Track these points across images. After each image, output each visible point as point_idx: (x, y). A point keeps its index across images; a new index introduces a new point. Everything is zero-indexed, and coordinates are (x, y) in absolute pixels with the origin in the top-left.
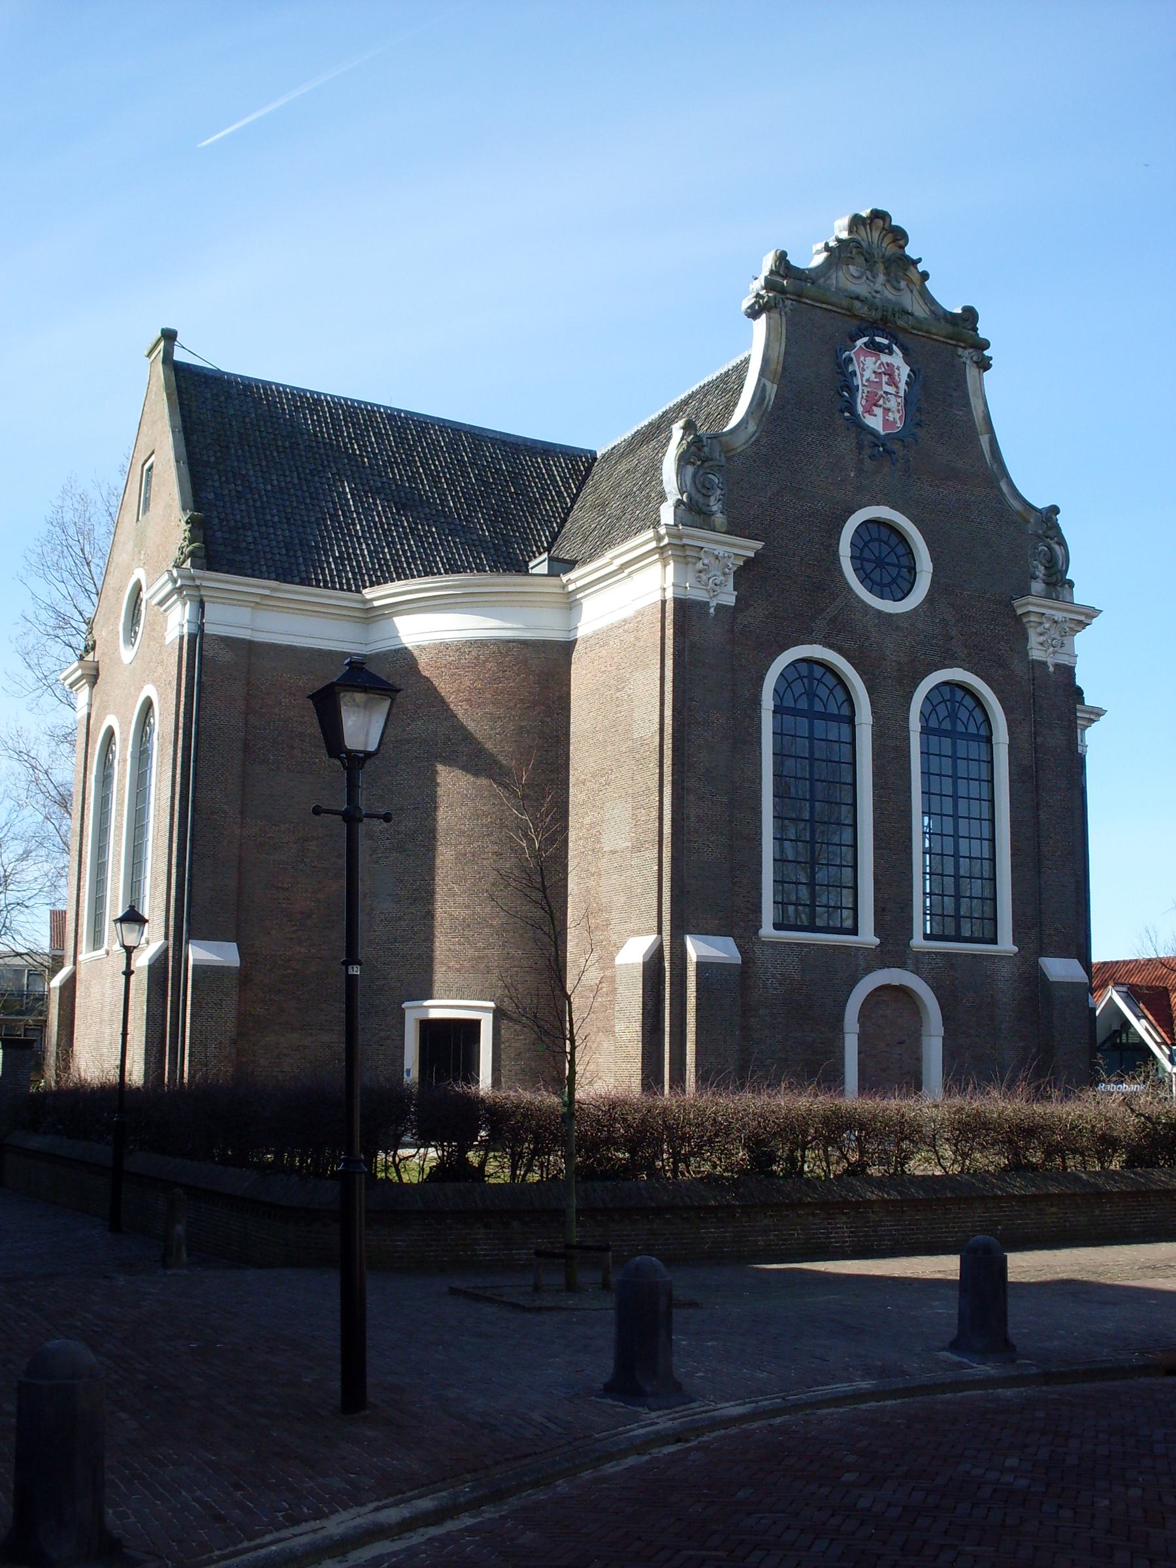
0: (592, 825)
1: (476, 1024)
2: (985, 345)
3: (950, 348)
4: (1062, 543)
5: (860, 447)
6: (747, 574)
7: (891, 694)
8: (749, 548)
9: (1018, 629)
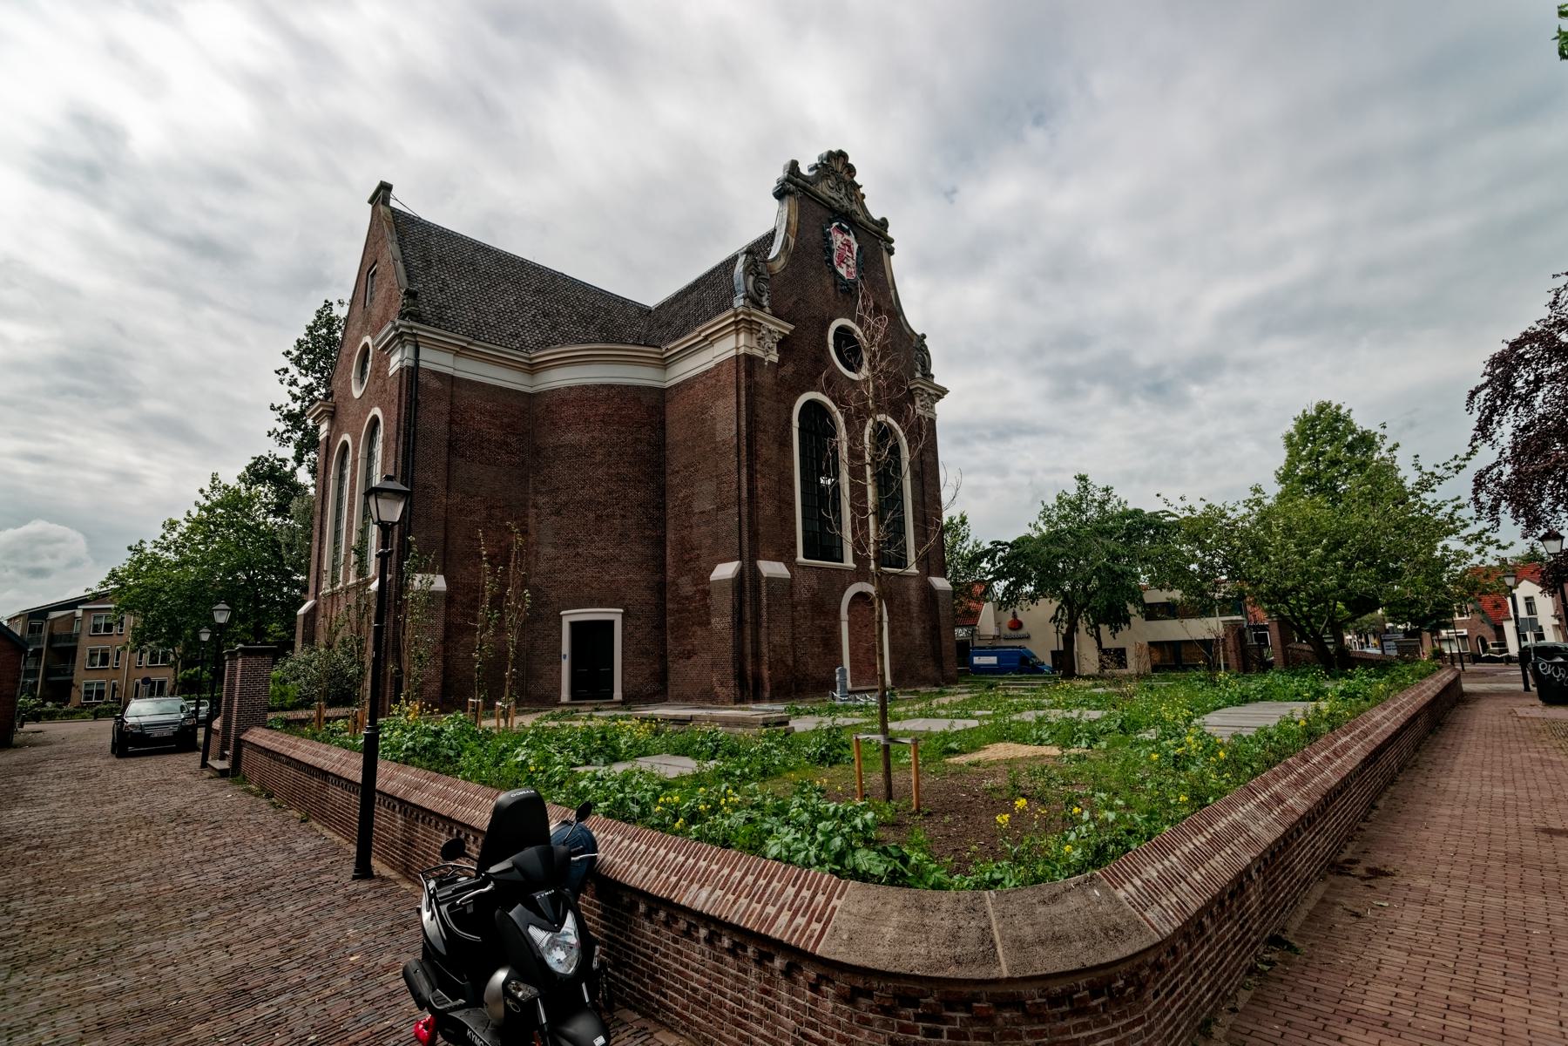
0: (686, 497)
1: (612, 622)
5: (836, 284)
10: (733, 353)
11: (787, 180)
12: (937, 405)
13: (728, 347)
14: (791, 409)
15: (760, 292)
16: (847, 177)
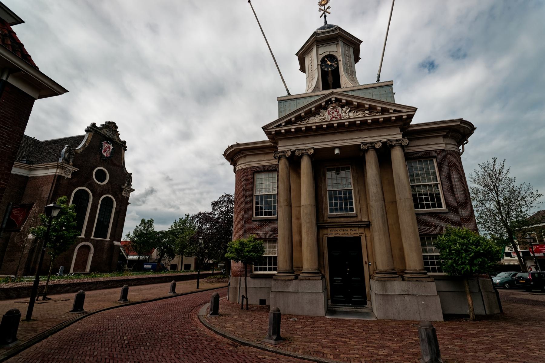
5: (101, 158)
6: (74, 174)
8: (76, 169)
9: (121, 190)
11: (91, 128)
13: (53, 172)
15: (69, 158)
16: (114, 129)
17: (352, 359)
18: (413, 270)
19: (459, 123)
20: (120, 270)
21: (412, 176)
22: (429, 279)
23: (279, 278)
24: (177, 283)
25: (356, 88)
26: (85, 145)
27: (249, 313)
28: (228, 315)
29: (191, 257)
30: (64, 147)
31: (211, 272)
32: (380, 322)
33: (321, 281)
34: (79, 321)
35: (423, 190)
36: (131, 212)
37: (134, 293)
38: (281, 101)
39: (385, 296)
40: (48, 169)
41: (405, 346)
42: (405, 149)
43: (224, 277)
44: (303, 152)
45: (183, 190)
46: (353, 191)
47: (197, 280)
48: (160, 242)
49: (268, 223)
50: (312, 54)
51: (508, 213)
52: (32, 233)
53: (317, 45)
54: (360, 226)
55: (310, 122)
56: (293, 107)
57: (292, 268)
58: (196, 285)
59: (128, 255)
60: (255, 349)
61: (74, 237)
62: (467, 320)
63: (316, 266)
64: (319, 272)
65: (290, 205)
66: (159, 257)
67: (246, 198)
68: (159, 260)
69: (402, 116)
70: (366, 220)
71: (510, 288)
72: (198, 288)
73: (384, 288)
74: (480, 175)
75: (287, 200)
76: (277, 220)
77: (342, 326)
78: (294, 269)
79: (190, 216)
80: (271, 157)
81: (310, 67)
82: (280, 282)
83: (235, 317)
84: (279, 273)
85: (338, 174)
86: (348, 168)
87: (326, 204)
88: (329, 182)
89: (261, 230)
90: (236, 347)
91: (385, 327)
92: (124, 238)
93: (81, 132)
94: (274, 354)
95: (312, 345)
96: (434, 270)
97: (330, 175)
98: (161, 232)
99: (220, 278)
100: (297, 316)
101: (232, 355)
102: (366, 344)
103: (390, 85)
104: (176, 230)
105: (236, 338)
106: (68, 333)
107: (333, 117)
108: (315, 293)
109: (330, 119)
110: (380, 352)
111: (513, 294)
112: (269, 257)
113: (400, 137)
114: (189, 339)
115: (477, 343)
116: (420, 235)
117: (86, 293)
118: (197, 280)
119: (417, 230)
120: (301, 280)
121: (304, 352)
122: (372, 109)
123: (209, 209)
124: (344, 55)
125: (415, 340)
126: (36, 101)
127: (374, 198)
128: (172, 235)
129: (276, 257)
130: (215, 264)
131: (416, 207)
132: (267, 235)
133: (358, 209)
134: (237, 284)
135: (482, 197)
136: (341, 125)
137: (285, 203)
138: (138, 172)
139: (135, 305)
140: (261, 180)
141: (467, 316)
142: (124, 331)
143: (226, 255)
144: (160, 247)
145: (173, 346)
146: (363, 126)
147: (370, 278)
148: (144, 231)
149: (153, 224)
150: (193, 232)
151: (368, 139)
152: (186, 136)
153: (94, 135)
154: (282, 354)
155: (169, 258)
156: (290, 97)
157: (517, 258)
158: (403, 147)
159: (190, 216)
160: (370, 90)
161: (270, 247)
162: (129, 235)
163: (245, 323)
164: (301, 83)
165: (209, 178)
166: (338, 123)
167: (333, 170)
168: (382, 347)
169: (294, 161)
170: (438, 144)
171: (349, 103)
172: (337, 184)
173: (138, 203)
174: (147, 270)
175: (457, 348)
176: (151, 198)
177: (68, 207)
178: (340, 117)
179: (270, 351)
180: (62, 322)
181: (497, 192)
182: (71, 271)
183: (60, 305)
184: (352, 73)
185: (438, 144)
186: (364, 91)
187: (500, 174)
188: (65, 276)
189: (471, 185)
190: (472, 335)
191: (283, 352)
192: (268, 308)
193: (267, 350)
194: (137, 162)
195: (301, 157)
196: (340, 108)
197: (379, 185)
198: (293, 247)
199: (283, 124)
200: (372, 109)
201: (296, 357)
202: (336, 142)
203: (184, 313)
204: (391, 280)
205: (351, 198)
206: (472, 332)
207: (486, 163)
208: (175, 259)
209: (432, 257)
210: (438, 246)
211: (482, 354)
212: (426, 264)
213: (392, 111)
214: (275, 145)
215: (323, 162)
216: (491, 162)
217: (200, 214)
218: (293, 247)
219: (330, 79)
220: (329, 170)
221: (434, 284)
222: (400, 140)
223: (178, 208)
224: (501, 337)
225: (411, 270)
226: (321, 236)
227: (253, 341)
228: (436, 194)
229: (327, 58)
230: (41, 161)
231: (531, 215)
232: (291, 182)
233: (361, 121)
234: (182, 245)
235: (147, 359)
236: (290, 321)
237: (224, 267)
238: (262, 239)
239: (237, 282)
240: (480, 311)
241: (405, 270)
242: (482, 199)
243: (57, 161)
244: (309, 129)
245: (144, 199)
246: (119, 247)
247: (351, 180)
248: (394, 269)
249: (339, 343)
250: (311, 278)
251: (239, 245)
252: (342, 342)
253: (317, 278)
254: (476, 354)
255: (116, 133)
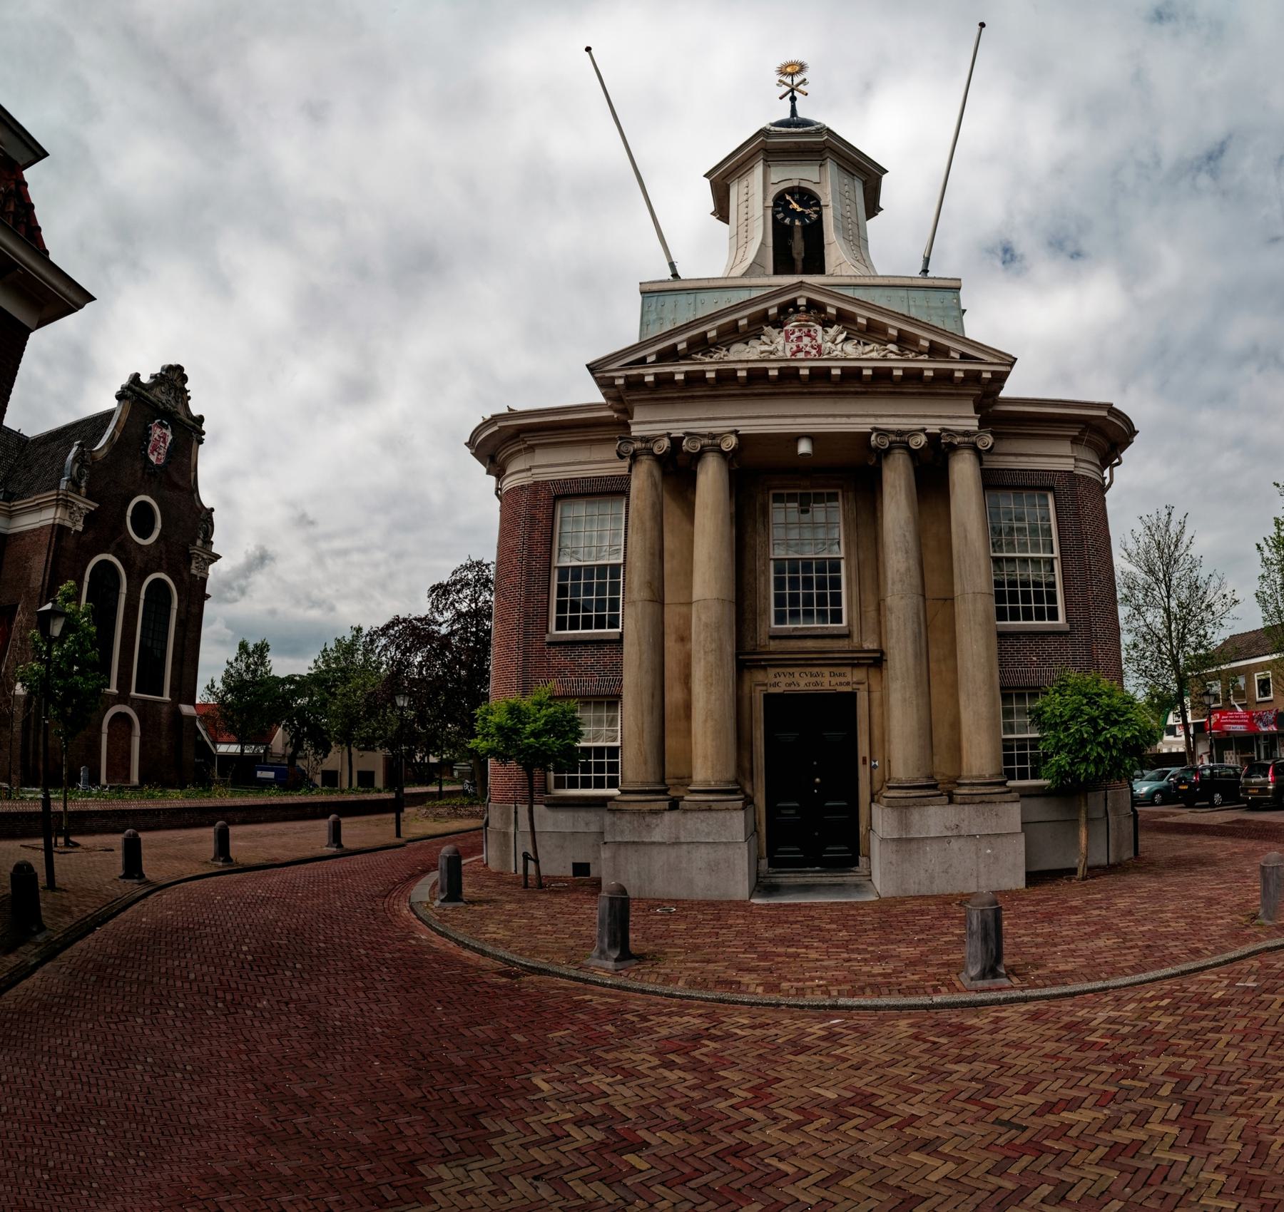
2: (204, 433)
3: (190, 432)
4: (212, 525)
6: (90, 518)
7: (135, 578)
8: (93, 506)
9: (189, 559)
10: (51, 522)
12: (211, 567)
13: (48, 517)
14: (85, 570)
16: (178, 384)
17: (809, 991)
18: (977, 777)
19: (1104, 413)
20: (203, 782)
21: (997, 531)
22: (1008, 797)
23: (624, 807)
24: (343, 820)
25: (867, 281)
26: (113, 435)
27: (544, 897)
28: (488, 902)
29: (373, 750)
30: (71, 447)
31: (434, 789)
32: (885, 905)
33: (742, 814)
34: (142, 902)
35: (1019, 573)
36: (212, 621)
37: (248, 842)
38: (649, 293)
39: (904, 843)
40: (41, 509)
41: (934, 951)
42: (985, 458)
43: (471, 804)
44: (706, 441)
45: (344, 553)
46: (843, 563)
47: (393, 815)
48: (289, 707)
49: (592, 650)
50: (750, 179)
51: (1182, 639)
52: (21, 680)
53: (765, 161)
54: (855, 664)
55: (731, 358)
56: (682, 312)
57: (662, 781)
58: (394, 827)
59: (215, 742)
60: (563, 983)
61: (97, 692)
62: (1070, 879)
63: (731, 773)
64: (736, 789)
65: (657, 599)
66: (290, 750)
67: (529, 574)
68: (293, 758)
69: (980, 372)
70: (874, 646)
71: (1163, 803)
72: (398, 835)
73: (904, 824)
74: (1142, 544)
75: (650, 584)
76: (619, 641)
77: (791, 919)
78: (667, 782)
79: (365, 632)
80: (609, 452)
81: (743, 210)
82: (627, 817)
83: (508, 907)
84: (624, 792)
85: (805, 511)
86: (832, 497)
87: (767, 598)
88: (776, 533)
89: (572, 671)
90: (517, 975)
91: (894, 916)
92: (202, 696)
93: (108, 402)
94: (614, 991)
95: (711, 966)
96: (1023, 775)
97: (781, 514)
98: (290, 679)
99: (462, 805)
100: (676, 902)
101: (506, 995)
102: (845, 955)
103: (954, 288)
104: (327, 672)
105: (515, 958)
106: (128, 924)
107: (799, 350)
108: (725, 843)
109: (789, 355)
110: (877, 970)
111: (1164, 815)
112: (596, 748)
113: (973, 424)
114: (393, 959)
115: (1078, 924)
116: (1002, 688)
117: (141, 835)
118: (393, 815)
119: (997, 675)
120: (686, 811)
121: (692, 984)
122: (904, 340)
123: (422, 607)
124: (840, 195)
125: (957, 935)
126: (32, 335)
127: (898, 586)
128: (319, 686)
129: (616, 748)
130: (445, 767)
131: (1001, 615)
132: (592, 685)
133: (855, 615)
134: (507, 824)
135: (1141, 596)
136: (821, 375)
137: (645, 594)
138: (228, 503)
139: (252, 874)
140: (576, 521)
141: (1073, 871)
142: (238, 932)
143: (473, 743)
144: (291, 721)
145: (358, 975)
146: (879, 384)
147: (872, 801)
148: (248, 677)
149: (269, 656)
150: (373, 679)
151: (891, 420)
152: (357, 391)
153: (133, 407)
154: (635, 991)
155: (316, 753)
156: (677, 285)
157: (1183, 738)
158: (979, 454)
159: (365, 632)
160: (902, 293)
161: (599, 722)
162: (213, 686)
163: (536, 923)
164: (715, 251)
165: (405, 512)
166: (811, 369)
167: (792, 498)
168: (881, 958)
169: (677, 469)
170: (1058, 457)
171: (843, 318)
172: (801, 543)
173: (228, 595)
174: (265, 784)
175: (1040, 940)
176: (260, 579)
177: (78, 611)
178: (819, 352)
179: (604, 985)
180: (110, 900)
181: (1168, 587)
182: (103, 780)
183: (92, 862)
184: (858, 242)
185: (1058, 457)
186: (888, 292)
187: (1176, 546)
188: (94, 791)
189: (1121, 564)
190: (1075, 910)
191: (637, 985)
192: (597, 883)
193: (596, 983)
194: (228, 475)
195: (698, 457)
196: (819, 328)
197: (913, 553)
198: (665, 721)
199: (651, 359)
200: (904, 340)
201: (672, 996)
202: (804, 421)
203: (372, 898)
204: (922, 802)
205: (836, 583)
206: (1074, 903)
207: (1155, 517)
208: (331, 755)
209: (1022, 744)
210: (1037, 716)
211: (1082, 945)
212: (1008, 760)
213: (957, 356)
214: (623, 417)
215: (760, 475)
216: (1164, 518)
217: (396, 621)
218: (665, 721)
219: (798, 246)
220: (778, 498)
221: (1015, 810)
222: (974, 433)
223: (332, 609)
224: (1121, 906)
225: (973, 777)
226: (746, 689)
227: (558, 964)
228: (1048, 585)
229: (792, 195)
230: (28, 491)
231: (1219, 643)
232: (665, 529)
233: (874, 369)
234: (346, 715)
235: (304, 997)
236: (656, 914)
237: (471, 776)
238: (574, 697)
239: (508, 818)
240: (1100, 858)
241: (959, 777)
242: (1141, 602)
243: (57, 486)
244: (727, 377)
245: (243, 582)
246: (192, 719)
247: (839, 533)
248: (931, 777)
249: (780, 959)
250: (714, 805)
251: (506, 716)
252: (787, 955)
253: (730, 805)
254: (1072, 946)
255: (183, 396)
